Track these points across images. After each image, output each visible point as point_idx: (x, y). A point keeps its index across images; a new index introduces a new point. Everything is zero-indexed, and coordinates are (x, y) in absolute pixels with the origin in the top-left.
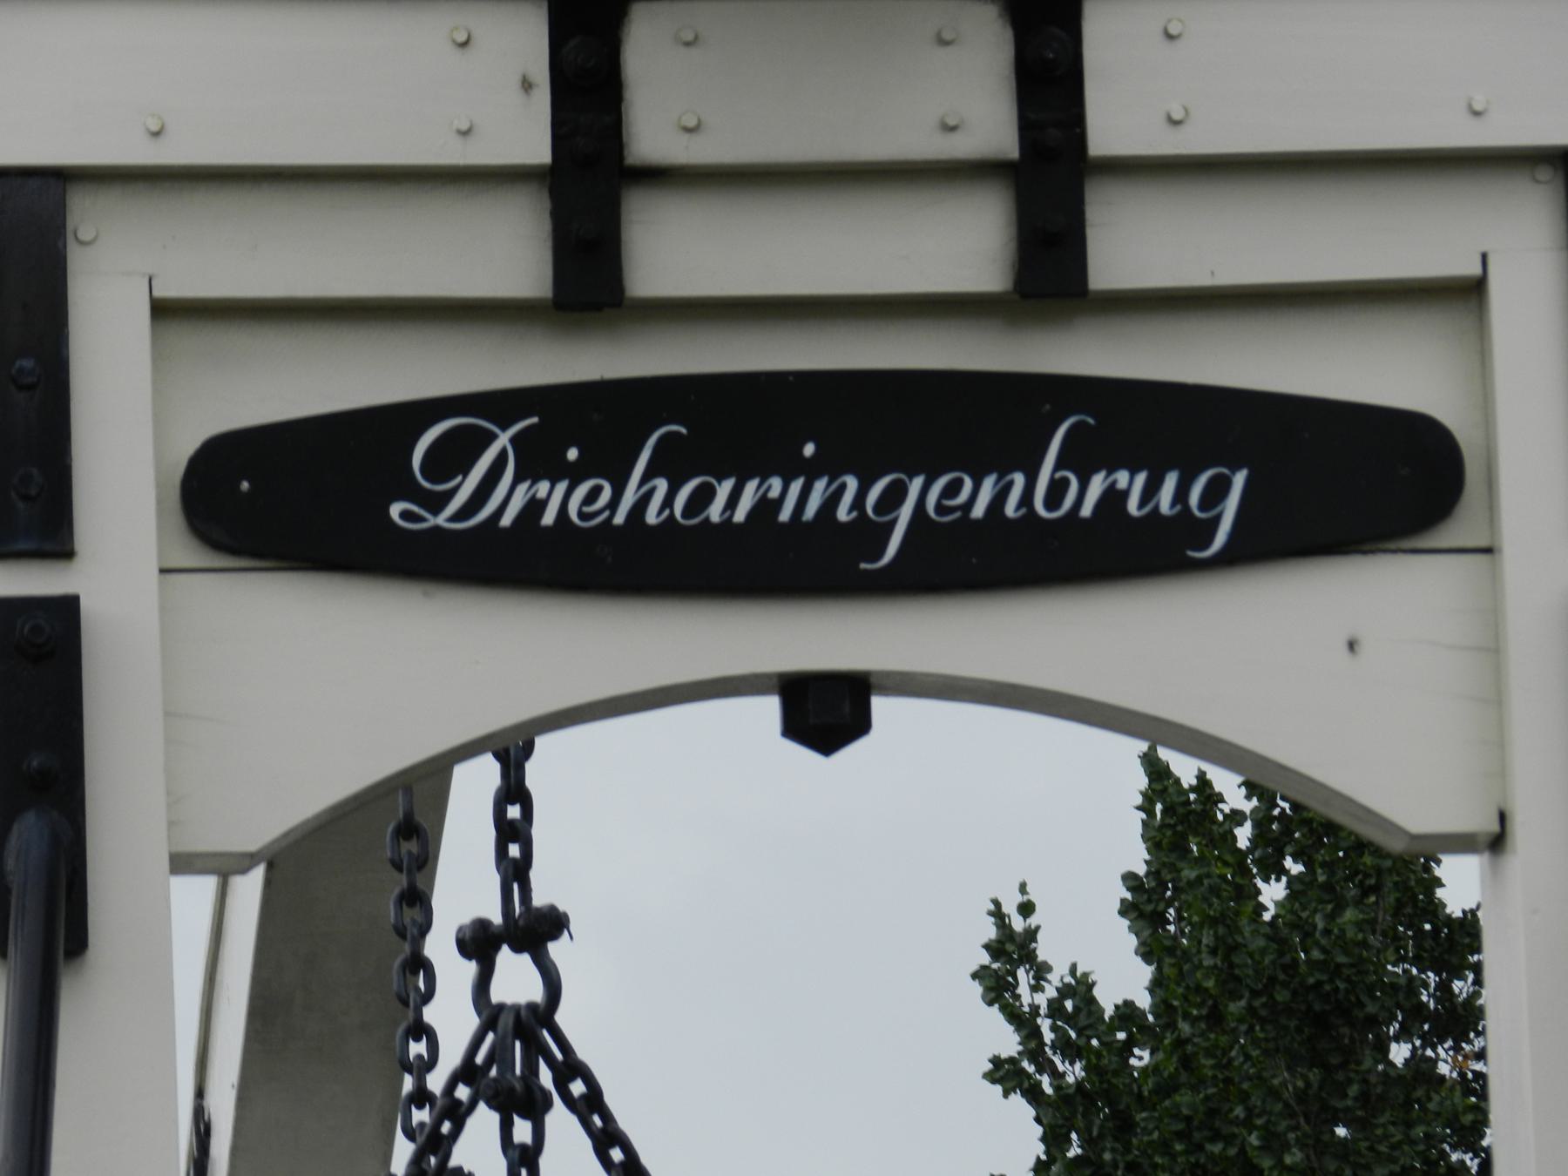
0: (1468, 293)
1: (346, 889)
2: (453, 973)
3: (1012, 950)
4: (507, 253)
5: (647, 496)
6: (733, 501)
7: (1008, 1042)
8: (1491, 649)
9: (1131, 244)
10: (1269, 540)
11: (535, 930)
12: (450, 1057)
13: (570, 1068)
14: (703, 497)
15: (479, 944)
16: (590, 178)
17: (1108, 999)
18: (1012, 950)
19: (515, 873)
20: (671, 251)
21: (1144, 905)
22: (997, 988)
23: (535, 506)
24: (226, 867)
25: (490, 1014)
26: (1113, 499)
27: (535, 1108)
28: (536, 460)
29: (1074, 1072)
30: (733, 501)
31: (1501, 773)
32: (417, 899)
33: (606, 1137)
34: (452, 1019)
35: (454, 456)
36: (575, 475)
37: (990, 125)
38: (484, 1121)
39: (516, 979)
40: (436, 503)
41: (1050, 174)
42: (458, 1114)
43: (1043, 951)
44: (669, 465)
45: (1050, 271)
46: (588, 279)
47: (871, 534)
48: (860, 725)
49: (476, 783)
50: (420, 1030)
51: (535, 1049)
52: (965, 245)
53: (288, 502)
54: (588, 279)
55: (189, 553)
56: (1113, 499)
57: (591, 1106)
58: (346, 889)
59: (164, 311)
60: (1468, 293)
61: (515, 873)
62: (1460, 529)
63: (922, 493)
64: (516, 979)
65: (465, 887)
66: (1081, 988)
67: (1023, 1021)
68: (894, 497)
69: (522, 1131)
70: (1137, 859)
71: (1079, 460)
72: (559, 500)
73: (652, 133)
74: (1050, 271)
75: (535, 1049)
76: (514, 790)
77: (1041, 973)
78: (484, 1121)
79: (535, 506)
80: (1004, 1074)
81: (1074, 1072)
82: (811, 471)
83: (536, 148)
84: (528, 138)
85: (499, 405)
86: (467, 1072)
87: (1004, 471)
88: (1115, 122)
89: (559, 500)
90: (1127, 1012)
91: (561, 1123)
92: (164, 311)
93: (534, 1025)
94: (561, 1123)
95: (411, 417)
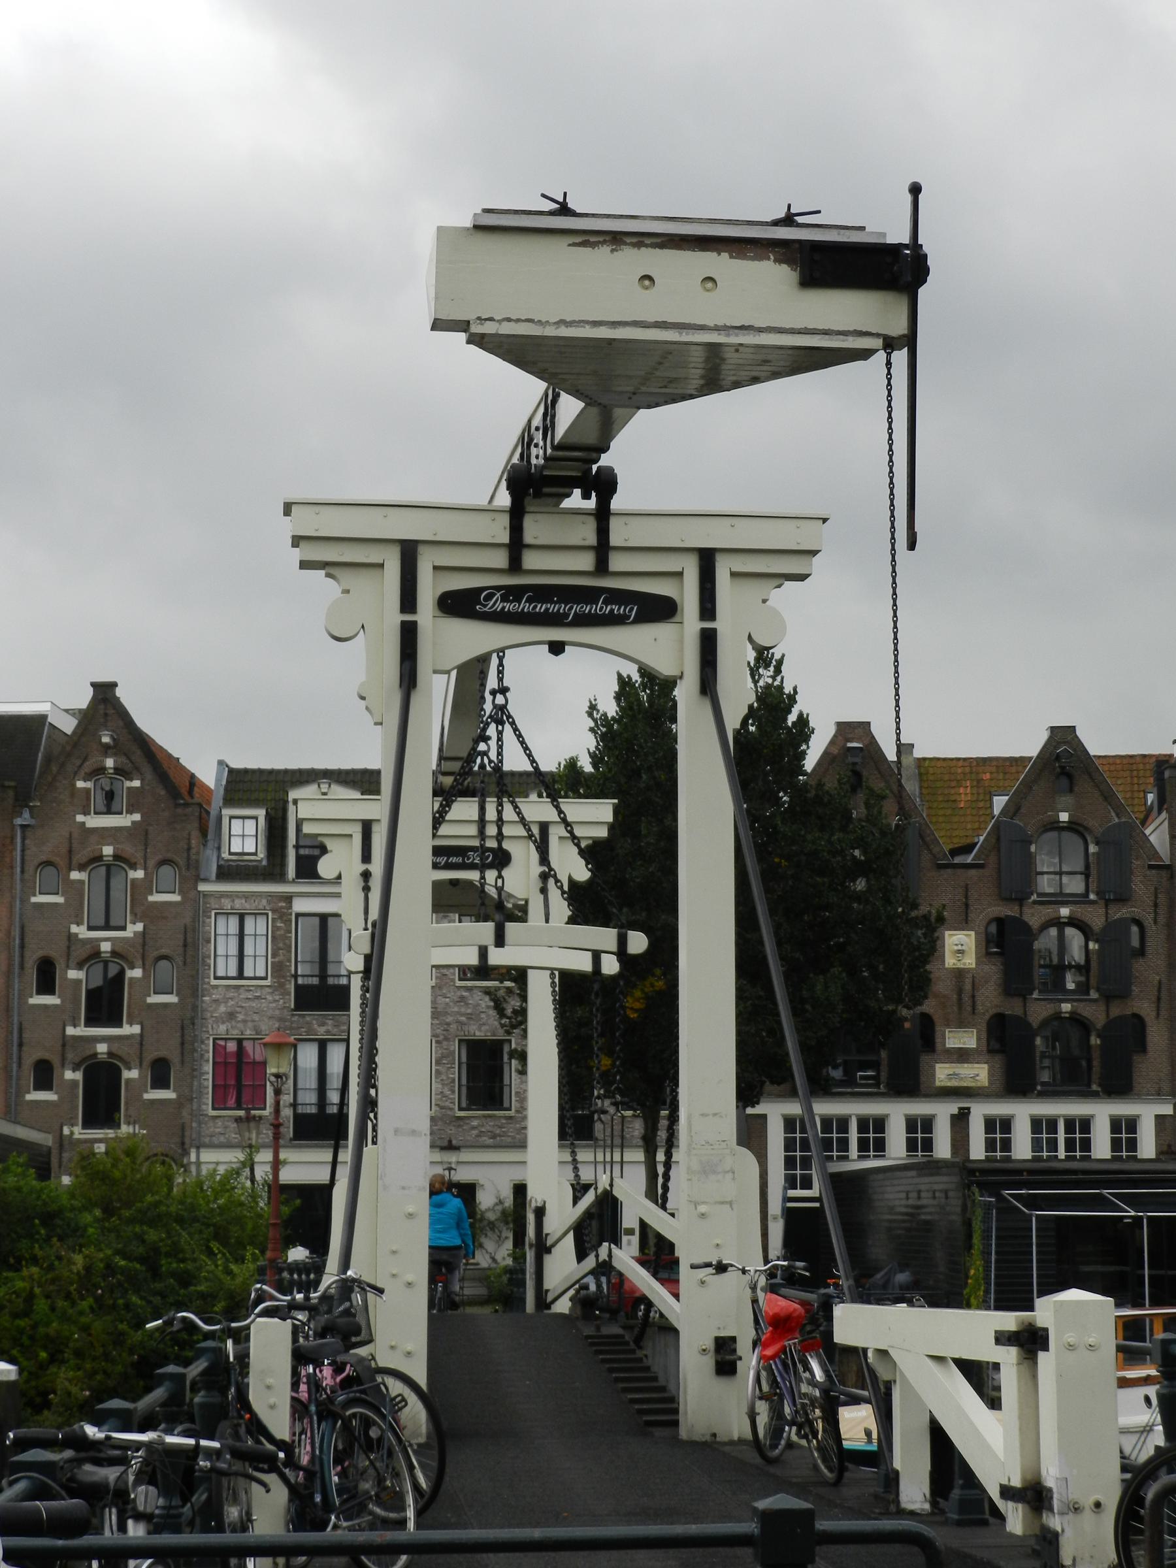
0: (680, 574)
1: (472, 674)
2: (488, 697)
3: (593, 707)
4: (500, 559)
5: (525, 606)
6: (541, 608)
7: (592, 724)
8: (681, 641)
9: (617, 563)
10: (642, 619)
11: (504, 690)
12: (488, 714)
13: (509, 716)
14: (535, 607)
15: (493, 693)
16: (516, 546)
17: (610, 716)
18: (593, 707)
19: (501, 680)
20: (531, 561)
21: (618, 697)
22: (590, 715)
23: (504, 608)
24: (448, 672)
25: (495, 706)
26: (612, 610)
27: (502, 723)
28: (504, 599)
29: (604, 730)
30: (541, 608)
31: (682, 665)
32: (483, 685)
33: (516, 730)
34: (488, 707)
35: (489, 597)
36: (512, 602)
37: (592, 540)
38: (493, 726)
39: (500, 699)
40: (485, 606)
41: (603, 549)
42: (488, 724)
43: (599, 707)
44: (529, 601)
45: (602, 567)
46: (515, 565)
47: (566, 615)
48: (563, 651)
49: (494, 661)
50: (483, 709)
51: (503, 713)
52: (586, 562)
53: (457, 605)
54: (515, 565)
55: (439, 613)
56: (612, 610)
57: (513, 724)
58: (472, 674)
59: (435, 568)
60: (680, 574)
61: (501, 680)
62: (676, 619)
63: (576, 608)
64: (500, 699)
65: (492, 682)
66: (605, 715)
67: (595, 720)
68: (571, 608)
69: (500, 728)
70: (617, 688)
71: (606, 603)
72: (509, 607)
73: (528, 538)
74: (602, 567)
75: (503, 713)
76: (501, 664)
77: (598, 711)
78: (493, 726)
79: (504, 608)
80: (591, 730)
81: (604, 730)
82: (556, 603)
83: (506, 540)
84: (505, 538)
85: (498, 588)
86: (490, 716)
87: (592, 604)
88: (615, 540)
89: (509, 607)
90: (613, 718)
91: (507, 727)
92: (435, 568)
93: (502, 708)
94: (507, 727)
95: (481, 590)
